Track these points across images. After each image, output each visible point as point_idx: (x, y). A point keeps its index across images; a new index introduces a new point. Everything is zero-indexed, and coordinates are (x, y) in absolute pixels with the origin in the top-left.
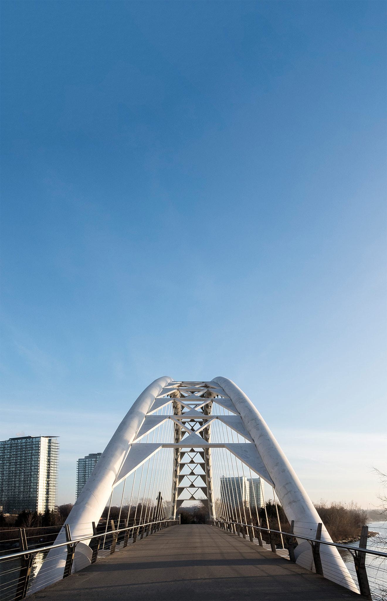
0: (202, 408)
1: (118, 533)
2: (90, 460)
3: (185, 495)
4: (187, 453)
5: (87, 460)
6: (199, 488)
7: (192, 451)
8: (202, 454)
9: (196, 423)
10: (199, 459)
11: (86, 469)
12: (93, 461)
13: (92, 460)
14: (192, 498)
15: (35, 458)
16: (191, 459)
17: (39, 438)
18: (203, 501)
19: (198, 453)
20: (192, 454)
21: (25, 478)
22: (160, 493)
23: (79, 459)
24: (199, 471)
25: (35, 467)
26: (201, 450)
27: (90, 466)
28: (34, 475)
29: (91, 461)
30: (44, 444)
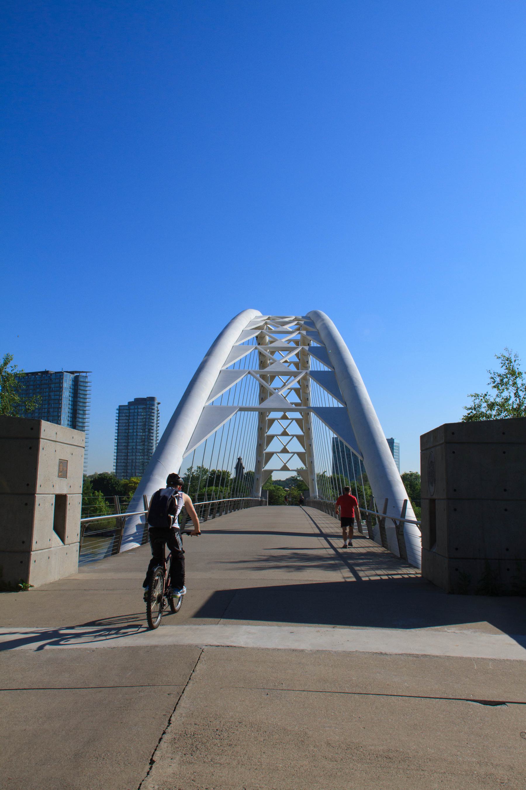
0: (297, 355)
1: (176, 500)
2: (136, 407)
3: (273, 464)
4: (277, 420)
5: (132, 407)
6: (294, 453)
7: (285, 417)
8: (298, 421)
9: (290, 364)
10: (295, 429)
11: (130, 421)
12: (141, 409)
13: (139, 407)
14: (285, 468)
15: (54, 404)
16: (284, 446)
17: (61, 374)
18: (299, 471)
19: (291, 364)
20: (285, 423)
21: (40, 413)
22: (239, 459)
23: (120, 406)
24: (296, 446)
25: (56, 393)
26: (298, 415)
27: (136, 417)
28: (53, 412)
29: (138, 409)
30: (67, 383)
